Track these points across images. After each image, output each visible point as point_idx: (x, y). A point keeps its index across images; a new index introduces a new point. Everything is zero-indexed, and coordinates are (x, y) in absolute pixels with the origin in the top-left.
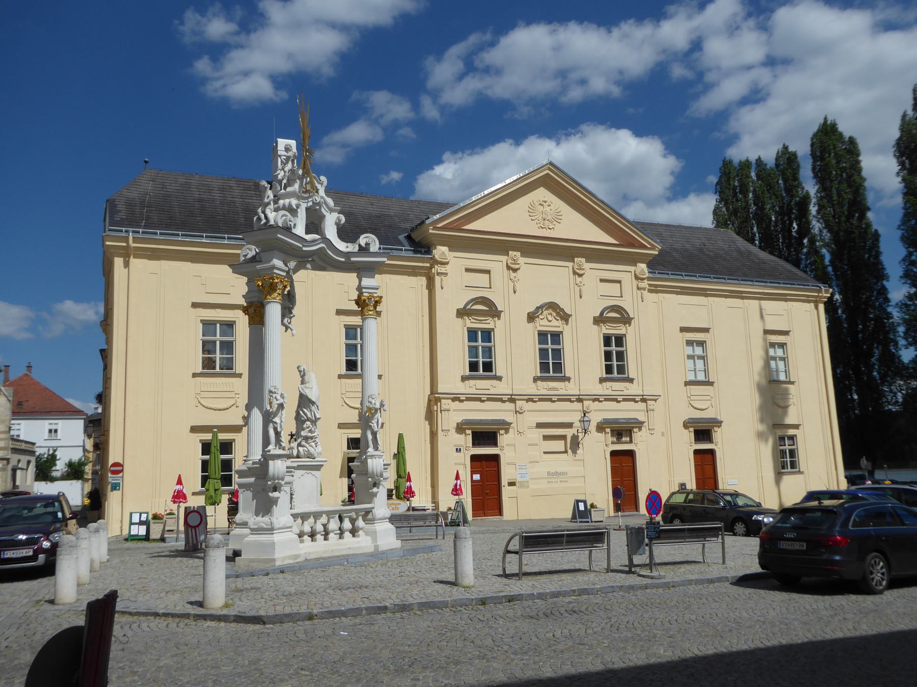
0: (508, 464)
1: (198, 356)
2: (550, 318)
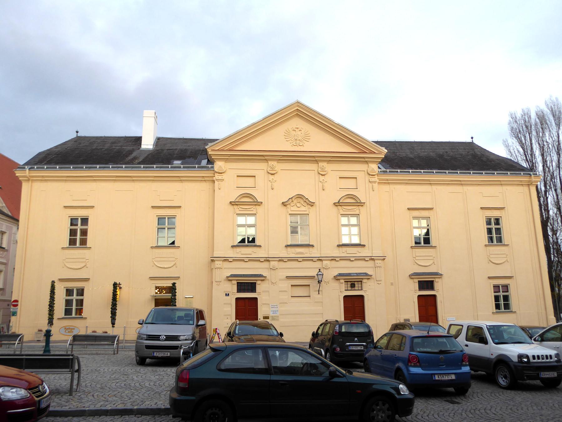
0: (264, 304)
1: (485, 236)
2: (298, 205)
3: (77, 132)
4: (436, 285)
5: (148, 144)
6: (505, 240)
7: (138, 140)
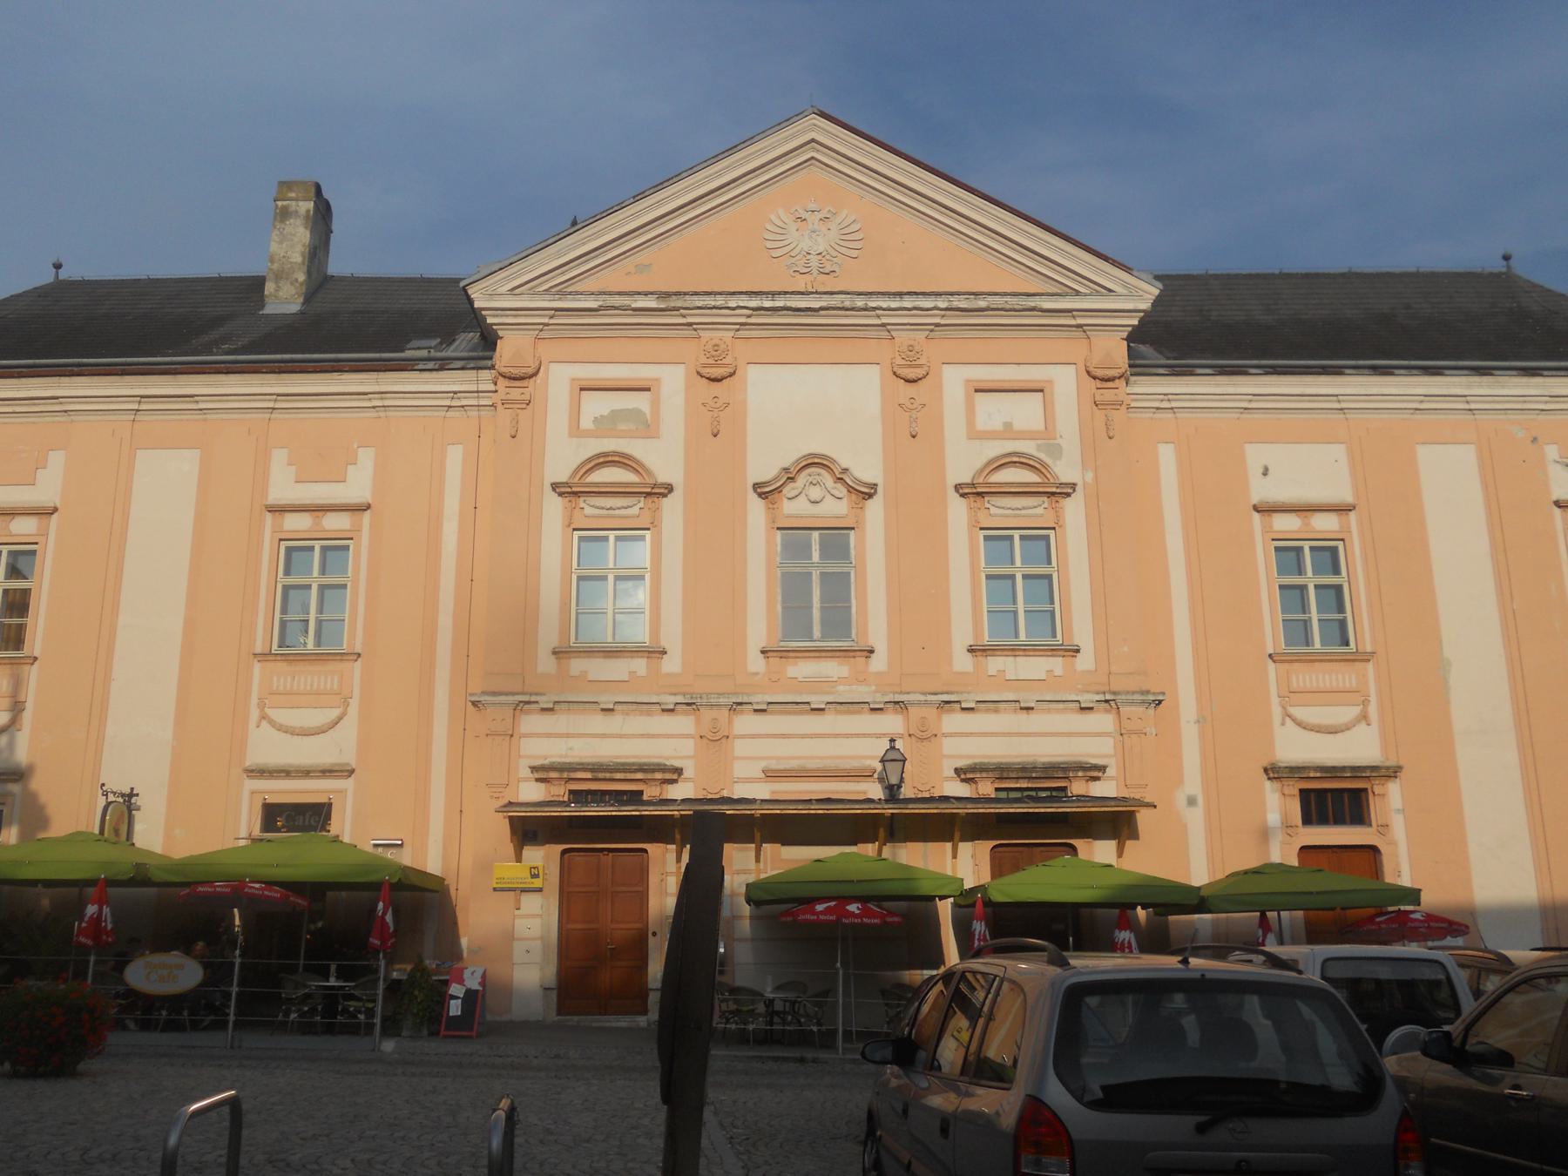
3: (58, 266)
4: (1375, 808)
5: (285, 299)
6: (1363, 633)
7: (254, 287)
